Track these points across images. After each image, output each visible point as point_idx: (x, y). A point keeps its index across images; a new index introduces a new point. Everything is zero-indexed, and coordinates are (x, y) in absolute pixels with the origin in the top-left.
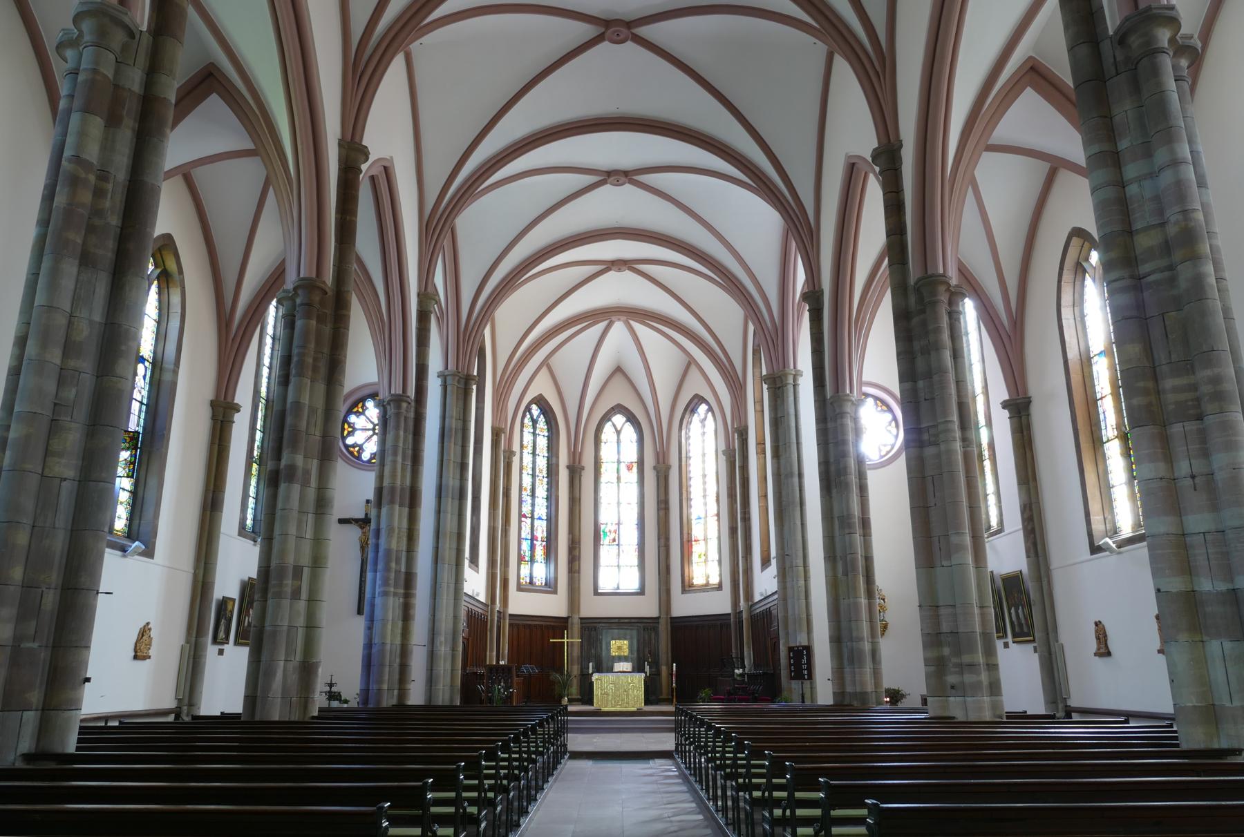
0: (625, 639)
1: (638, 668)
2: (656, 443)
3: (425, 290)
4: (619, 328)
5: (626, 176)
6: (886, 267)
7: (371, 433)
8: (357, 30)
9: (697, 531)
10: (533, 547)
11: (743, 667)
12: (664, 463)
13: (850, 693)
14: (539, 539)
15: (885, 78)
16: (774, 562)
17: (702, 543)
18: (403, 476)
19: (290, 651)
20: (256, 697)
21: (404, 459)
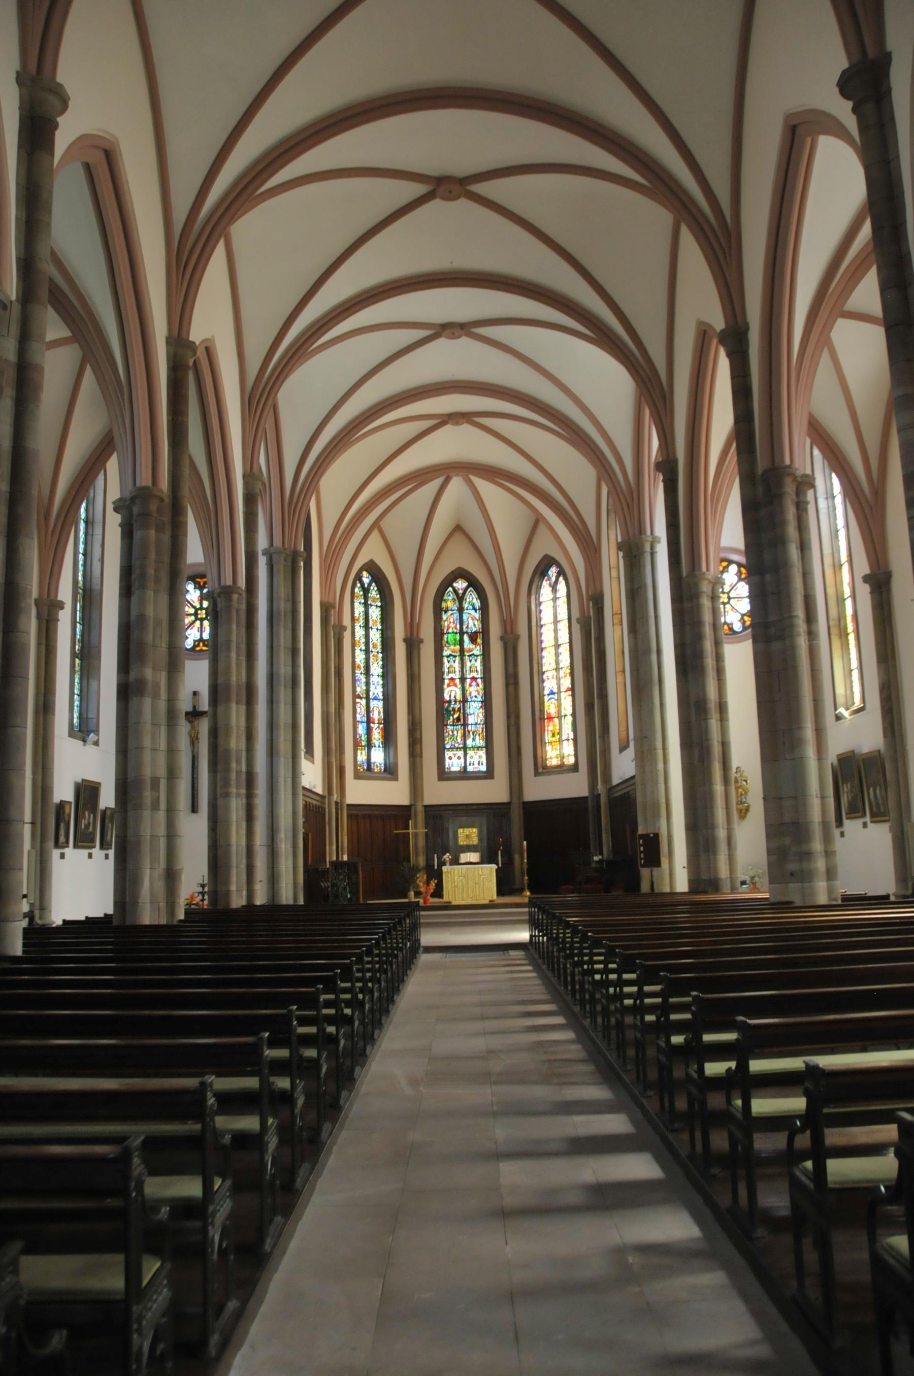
0: (473, 827)
1: (488, 858)
2: (502, 611)
3: (251, 471)
4: (457, 484)
5: (462, 329)
6: (733, 453)
7: (198, 623)
8: (180, 216)
9: (550, 707)
10: (369, 731)
11: (601, 853)
12: (512, 632)
13: (704, 880)
14: (376, 722)
15: (730, 255)
16: (632, 744)
17: (556, 720)
18: (239, 673)
19: (154, 860)
20: (125, 903)
21: (238, 655)
